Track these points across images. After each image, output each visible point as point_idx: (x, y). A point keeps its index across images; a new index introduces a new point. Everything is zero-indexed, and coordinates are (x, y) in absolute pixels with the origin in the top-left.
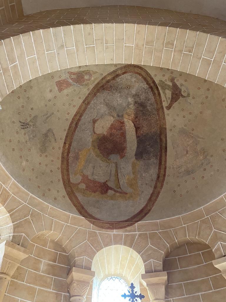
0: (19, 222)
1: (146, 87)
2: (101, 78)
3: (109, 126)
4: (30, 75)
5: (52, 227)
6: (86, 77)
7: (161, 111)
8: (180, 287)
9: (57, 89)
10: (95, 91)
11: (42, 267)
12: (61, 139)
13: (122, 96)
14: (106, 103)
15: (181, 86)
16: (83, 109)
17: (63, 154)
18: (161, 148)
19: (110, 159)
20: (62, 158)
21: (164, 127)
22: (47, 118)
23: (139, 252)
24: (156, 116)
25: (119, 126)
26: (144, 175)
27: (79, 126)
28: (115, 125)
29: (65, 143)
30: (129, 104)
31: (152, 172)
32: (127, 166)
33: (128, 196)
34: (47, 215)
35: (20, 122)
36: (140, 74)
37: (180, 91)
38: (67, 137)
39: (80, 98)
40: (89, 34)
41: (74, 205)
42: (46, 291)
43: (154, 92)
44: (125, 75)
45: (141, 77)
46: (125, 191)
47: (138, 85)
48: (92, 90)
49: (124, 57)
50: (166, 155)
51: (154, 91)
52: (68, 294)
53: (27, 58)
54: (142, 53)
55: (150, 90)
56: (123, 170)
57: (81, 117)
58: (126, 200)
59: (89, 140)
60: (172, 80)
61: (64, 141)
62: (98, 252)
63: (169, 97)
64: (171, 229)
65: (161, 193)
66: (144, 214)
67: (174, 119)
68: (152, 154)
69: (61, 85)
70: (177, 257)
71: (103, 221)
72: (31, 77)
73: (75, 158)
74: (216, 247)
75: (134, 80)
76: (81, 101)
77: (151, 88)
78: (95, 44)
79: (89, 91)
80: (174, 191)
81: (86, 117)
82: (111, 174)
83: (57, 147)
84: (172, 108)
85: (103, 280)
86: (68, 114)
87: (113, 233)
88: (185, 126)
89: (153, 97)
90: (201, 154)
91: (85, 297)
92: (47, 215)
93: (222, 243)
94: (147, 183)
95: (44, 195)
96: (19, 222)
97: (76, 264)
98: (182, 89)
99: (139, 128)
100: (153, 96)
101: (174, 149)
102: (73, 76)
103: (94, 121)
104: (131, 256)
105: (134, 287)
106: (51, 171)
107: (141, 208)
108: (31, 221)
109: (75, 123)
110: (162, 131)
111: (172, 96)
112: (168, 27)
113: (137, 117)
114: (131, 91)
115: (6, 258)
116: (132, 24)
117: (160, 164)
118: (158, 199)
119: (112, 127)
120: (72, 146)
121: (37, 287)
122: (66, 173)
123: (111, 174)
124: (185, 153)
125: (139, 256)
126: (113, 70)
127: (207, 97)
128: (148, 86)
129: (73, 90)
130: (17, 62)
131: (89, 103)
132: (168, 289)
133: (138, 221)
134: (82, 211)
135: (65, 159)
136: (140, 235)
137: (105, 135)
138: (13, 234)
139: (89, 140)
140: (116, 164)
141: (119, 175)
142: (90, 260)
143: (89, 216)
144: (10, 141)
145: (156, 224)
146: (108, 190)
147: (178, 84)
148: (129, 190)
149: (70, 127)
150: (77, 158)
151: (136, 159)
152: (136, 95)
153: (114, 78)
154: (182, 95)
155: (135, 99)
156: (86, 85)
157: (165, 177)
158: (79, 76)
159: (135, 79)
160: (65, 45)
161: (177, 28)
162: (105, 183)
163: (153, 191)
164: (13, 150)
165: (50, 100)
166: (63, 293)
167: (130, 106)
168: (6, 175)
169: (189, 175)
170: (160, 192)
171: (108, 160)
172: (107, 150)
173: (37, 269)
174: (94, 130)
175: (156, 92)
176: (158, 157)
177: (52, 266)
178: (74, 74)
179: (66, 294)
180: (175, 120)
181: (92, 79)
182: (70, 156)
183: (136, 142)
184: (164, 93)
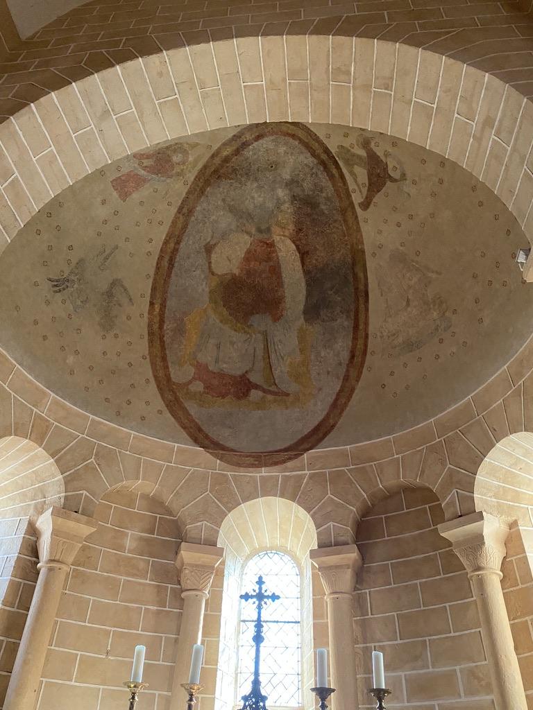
0: (73, 471)
1: (312, 162)
2: (208, 156)
3: (243, 256)
4: (49, 188)
5: (138, 473)
6: (176, 158)
7: (349, 213)
8: (384, 570)
9: (117, 196)
10: (200, 185)
11: (129, 543)
12: (142, 296)
13: (263, 187)
14: (229, 205)
15: (386, 157)
16: (180, 225)
17: (150, 326)
18: (356, 294)
19: (252, 325)
20: (149, 335)
21: (360, 247)
22: (106, 258)
23: (308, 510)
24: (341, 225)
25: (264, 253)
26: (323, 354)
27: (176, 265)
28: (255, 251)
29: (152, 304)
30: (279, 204)
31: (341, 347)
32: (288, 336)
33: (291, 398)
34: (128, 452)
35: (50, 280)
36: (293, 136)
37: (384, 169)
38: (154, 289)
39: (169, 204)
40: (160, 74)
41: (182, 427)
42: (140, 584)
43: (331, 172)
44: (261, 141)
45: (297, 143)
46: (285, 390)
47: (294, 161)
48: (193, 183)
49: (246, 111)
50: (367, 310)
51: (331, 170)
52: (178, 586)
53: (34, 159)
54: (286, 96)
55: (322, 169)
56: (279, 347)
57: (179, 244)
58: (287, 408)
59: (203, 290)
60: (366, 144)
61: (148, 299)
62: (229, 511)
63: (364, 182)
64: (371, 463)
65: (356, 391)
66: (321, 435)
67: (378, 230)
68: (338, 309)
69: (125, 183)
70: (383, 516)
71: (242, 452)
72: (51, 192)
73: (177, 331)
74: (448, 498)
75: (282, 150)
76: (174, 210)
77: (323, 163)
78: (177, 93)
79: (189, 186)
80: (384, 386)
81: (191, 242)
82: (254, 356)
83: (136, 315)
84: (372, 205)
85: (249, 557)
86: (150, 241)
87: (261, 474)
88: (402, 244)
89: (329, 184)
90: (434, 306)
91: (207, 593)
92: (128, 452)
93: (459, 491)
94: (330, 369)
95: (118, 414)
96: (73, 471)
97: (188, 536)
98: (388, 163)
99: (307, 252)
100: (329, 182)
101: (382, 295)
102: (146, 162)
103: (209, 249)
104: (297, 516)
105: (247, 594)
106: (130, 364)
107: (316, 423)
108: (97, 466)
109: (167, 258)
110: (357, 259)
111: (369, 179)
112: (333, 35)
113: (300, 230)
114: (280, 175)
115: (57, 536)
116: (251, 39)
117: (356, 327)
118: (350, 403)
119: (249, 256)
120: (167, 308)
121: (121, 577)
122: (162, 364)
123: (254, 356)
124: (405, 303)
125: (309, 516)
126: (232, 135)
127: (441, 182)
128: (315, 160)
129: (152, 190)
130: (17, 174)
131: (191, 212)
132: (361, 575)
133: (311, 448)
134: (199, 436)
135: (157, 337)
136: (312, 477)
137: (235, 274)
138: (63, 494)
139: (203, 290)
140: (265, 335)
141: (273, 356)
142: (215, 527)
143: (212, 446)
144: (36, 322)
145: (343, 454)
146: (250, 390)
147: (380, 153)
148: (293, 387)
149: (158, 268)
150: (180, 330)
151: (306, 320)
152: (292, 183)
153: (237, 152)
154: (390, 177)
155: (290, 190)
156: (178, 174)
157: (366, 355)
158: (161, 160)
159: (285, 149)
160: (112, 110)
161: (352, 36)
162: (244, 375)
163: (341, 386)
164: (45, 338)
165: (105, 222)
166: (170, 586)
167: (282, 208)
168: (37, 388)
169: (411, 351)
170: (354, 389)
171: (246, 329)
172: (244, 307)
173: (121, 548)
174: (210, 267)
175: (335, 171)
176: (352, 314)
177: (146, 540)
178: (148, 157)
179: (176, 586)
180: (380, 232)
181: (191, 159)
182: (165, 328)
183: (303, 284)
184: (352, 173)
